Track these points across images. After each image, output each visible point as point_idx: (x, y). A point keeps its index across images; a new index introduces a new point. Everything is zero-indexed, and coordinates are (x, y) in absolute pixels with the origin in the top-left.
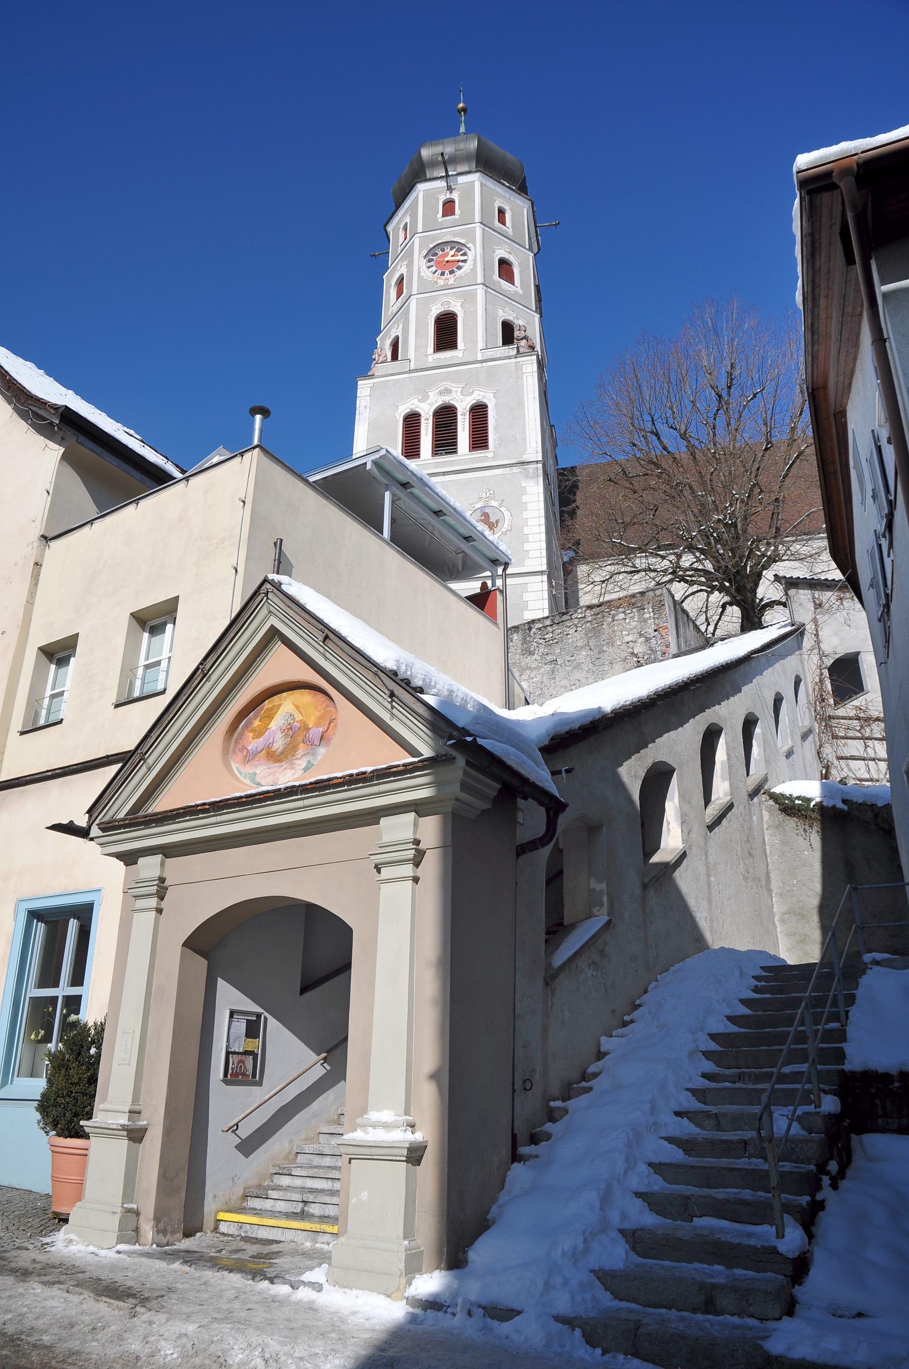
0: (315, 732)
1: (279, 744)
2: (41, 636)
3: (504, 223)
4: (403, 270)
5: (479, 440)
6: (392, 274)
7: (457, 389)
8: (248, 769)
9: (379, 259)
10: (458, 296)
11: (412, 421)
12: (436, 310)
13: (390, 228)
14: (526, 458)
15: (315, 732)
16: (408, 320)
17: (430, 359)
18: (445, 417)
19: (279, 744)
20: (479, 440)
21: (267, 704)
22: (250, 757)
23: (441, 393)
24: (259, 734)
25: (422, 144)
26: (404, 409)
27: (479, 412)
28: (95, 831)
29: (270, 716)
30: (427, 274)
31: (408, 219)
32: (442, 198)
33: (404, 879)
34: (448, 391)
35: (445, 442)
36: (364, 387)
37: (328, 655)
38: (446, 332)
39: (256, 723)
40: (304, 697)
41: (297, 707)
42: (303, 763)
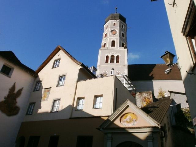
0: (134, 120)
1: (128, 120)
2: (77, 96)
3: (123, 27)
4: (107, 33)
5: (118, 62)
6: (104, 33)
7: (115, 53)
8: (124, 123)
9: (102, 30)
10: (115, 38)
11: (107, 57)
12: (112, 40)
13: (104, 26)
14: (125, 65)
15: (134, 120)
16: (106, 41)
17: (111, 48)
18: (112, 57)
19: (128, 120)
20: (118, 62)
21: (126, 115)
22: (124, 122)
23: (112, 53)
24: (125, 119)
25: (164, 72)
26: (106, 55)
27: (118, 57)
28: (101, 129)
29: (127, 116)
30: (111, 34)
31: (108, 25)
32: (113, 23)
33: (110, 141)
34: (113, 53)
35: (112, 61)
36: (100, 51)
37: (162, 119)
38: (113, 44)
39: (124, 117)
40: (132, 115)
41: (131, 116)
42: (133, 124)
